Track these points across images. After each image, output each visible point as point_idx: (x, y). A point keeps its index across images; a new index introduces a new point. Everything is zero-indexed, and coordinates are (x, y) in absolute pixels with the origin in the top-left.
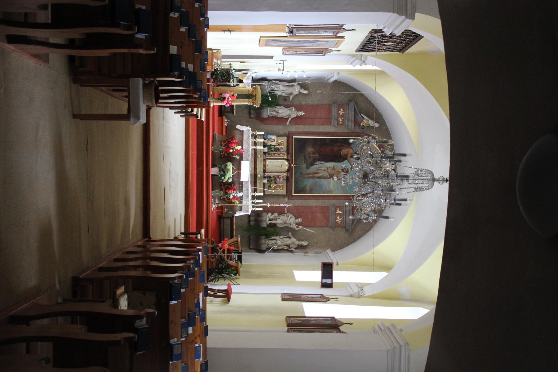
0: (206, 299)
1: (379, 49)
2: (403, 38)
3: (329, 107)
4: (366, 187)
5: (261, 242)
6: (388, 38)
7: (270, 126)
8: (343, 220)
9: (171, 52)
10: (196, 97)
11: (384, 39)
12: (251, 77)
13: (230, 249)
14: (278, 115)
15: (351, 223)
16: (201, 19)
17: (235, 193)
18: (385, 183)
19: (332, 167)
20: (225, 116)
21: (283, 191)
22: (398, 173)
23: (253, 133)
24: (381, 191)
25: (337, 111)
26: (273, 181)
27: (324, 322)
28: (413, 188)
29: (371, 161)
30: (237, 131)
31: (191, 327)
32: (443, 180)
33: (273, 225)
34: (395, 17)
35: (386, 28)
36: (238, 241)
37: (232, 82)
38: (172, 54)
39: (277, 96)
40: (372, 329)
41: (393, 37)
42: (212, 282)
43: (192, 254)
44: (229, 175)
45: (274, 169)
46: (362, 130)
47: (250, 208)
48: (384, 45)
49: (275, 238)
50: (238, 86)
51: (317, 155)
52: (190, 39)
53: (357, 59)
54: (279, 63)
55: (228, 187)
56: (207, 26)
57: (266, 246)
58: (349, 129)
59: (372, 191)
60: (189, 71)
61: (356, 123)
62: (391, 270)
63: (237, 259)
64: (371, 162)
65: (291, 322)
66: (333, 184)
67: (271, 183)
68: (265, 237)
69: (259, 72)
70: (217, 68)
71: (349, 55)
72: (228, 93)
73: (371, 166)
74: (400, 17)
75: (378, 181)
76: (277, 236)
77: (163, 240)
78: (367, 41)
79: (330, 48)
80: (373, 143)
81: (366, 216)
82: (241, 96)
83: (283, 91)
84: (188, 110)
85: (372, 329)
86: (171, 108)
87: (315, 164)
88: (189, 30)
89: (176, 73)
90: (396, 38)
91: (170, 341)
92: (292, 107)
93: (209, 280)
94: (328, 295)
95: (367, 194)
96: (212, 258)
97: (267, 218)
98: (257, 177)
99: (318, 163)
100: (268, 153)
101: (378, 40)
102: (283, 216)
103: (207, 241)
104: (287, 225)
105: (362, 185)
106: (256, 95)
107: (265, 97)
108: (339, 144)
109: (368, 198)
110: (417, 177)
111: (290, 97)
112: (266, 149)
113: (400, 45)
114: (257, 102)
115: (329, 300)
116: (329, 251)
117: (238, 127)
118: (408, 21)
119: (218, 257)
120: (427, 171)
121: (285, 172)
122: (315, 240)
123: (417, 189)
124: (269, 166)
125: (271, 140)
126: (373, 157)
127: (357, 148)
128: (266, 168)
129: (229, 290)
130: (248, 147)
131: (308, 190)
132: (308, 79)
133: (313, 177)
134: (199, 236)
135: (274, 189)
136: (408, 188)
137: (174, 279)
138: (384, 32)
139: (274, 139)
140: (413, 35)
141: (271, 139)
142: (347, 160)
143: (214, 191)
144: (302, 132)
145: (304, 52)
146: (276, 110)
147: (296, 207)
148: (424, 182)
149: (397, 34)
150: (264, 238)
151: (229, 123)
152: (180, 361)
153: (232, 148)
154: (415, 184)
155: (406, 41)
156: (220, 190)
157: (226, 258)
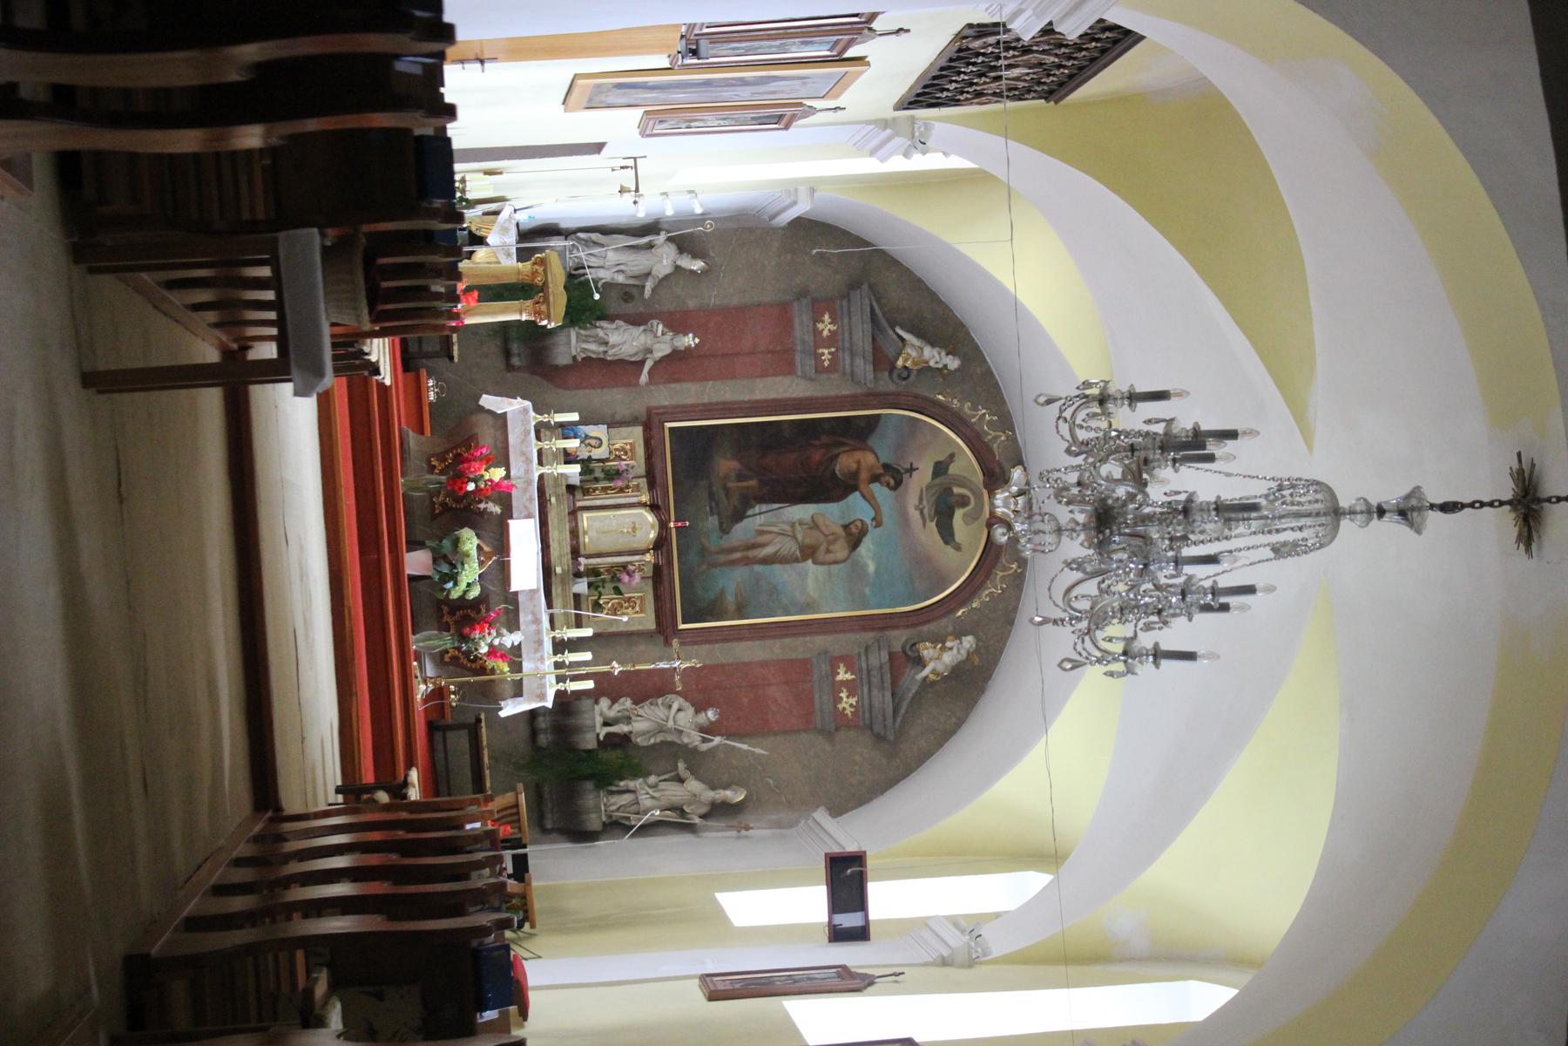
1: (979, 94)
3: (784, 309)
6: (1016, 53)
7: (580, 393)
8: (863, 706)
12: (514, 222)
14: (605, 352)
15: (891, 713)
17: (495, 634)
23: (540, 418)
25: (811, 325)
26: (609, 586)
32: (1369, 512)
33: (617, 740)
36: (517, 805)
41: (1035, 48)
43: (468, 849)
44: (470, 573)
45: (606, 544)
46: (904, 383)
47: (551, 685)
49: (631, 784)
50: (469, 258)
51: (753, 483)
53: (897, 134)
54: (622, 168)
55: (466, 616)
57: (600, 817)
61: (882, 361)
68: (595, 784)
69: (540, 204)
71: (868, 122)
76: (634, 779)
79: (808, 103)
87: (750, 512)
90: (1043, 52)
92: (655, 322)
97: (598, 719)
99: (757, 509)
100: (581, 487)
102: (652, 707)
104: (670, 738)
106: (545, 284)
108: (825, 439)
111: (644, 287)
114: (552, 310)
115: (871, 984)
116: (821, 815)
117: (488, 401)
121: (648, 551)
123: (1282, 549)
125: (587, 441)
128: (581, 539)
131: (732, 607)
132: (700, 220)
133: (748, 561)
139: (601, 437)
140: (1107, 34)
141: (587, 437)
142: (857, 494)
143: (418, 636)
144: (693, 406)
145: (716, 123)
146: (597, 335)
148: (1303, 521)
149: (1069, 33)
151: (442, 388)
153: (472, 476)
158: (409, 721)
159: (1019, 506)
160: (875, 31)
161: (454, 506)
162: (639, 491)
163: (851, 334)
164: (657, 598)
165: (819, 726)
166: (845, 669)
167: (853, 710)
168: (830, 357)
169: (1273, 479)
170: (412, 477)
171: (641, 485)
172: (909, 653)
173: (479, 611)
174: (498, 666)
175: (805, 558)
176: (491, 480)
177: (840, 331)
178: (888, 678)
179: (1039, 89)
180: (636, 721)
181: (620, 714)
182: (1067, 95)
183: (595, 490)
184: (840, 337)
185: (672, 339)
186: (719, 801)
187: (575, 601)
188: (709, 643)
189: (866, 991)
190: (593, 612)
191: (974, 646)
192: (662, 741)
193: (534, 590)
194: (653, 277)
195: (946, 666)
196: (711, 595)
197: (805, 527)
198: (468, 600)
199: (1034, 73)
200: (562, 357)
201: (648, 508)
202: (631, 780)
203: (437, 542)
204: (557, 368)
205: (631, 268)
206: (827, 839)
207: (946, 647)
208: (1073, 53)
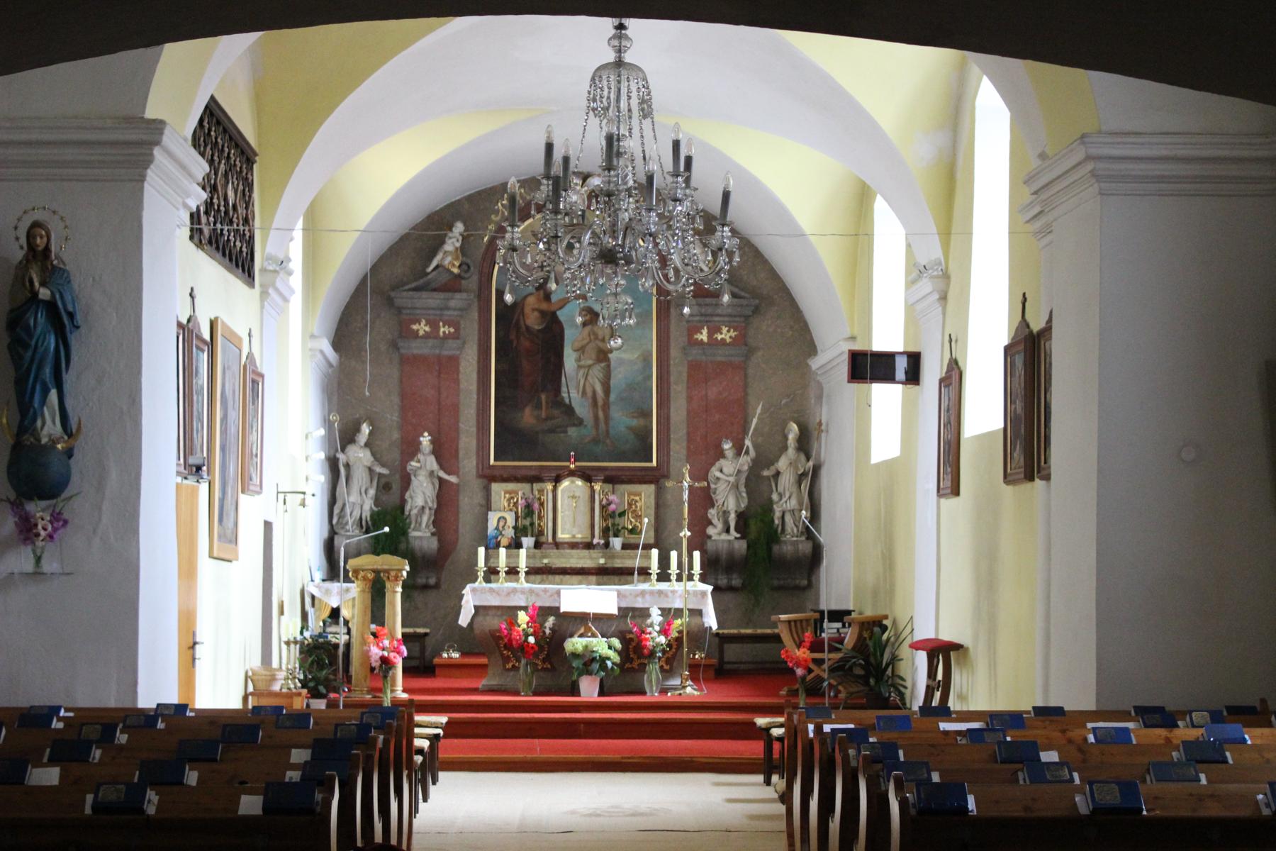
0: (957, 712)
2: (216, 154)
3: (406, 361)
4: (639, 256)
5: (788, 556)
6: (216, 197)
7: (461, 530)
8: (729, 322)
10: (384, 739)
11: (219, 206)
13: (811, 642)
14: (430, 509)
16: (161, 725)
18: (629, 203)
19: (579, 353)
20: (434, 657)
21: (645, 495)
22: (600, 164)
23: (480, 579)
24: (653, 214)
26: (617, 520)
27: (1020, 376)
28: (641, 123)
29: (565, 243)
31: (1039, 757)
36: (789, 622)
38: (264, 809)
40: (1039, 240)
41: (213, 182)
43: (830, 750)
44: (604, 647)
45: (584, 520)
46: (472, 268)
47: (695, 586)
48: (234, 207)
49: (777, 514)
51: (543, 397)
52: (218, 758)
53: (273, 285)
54: (285, 503)
55: (634, 651)
56: (181, 708)
57: (802, 542)
59: (651, 239)
60: (309, 759)
61: (452, 285)
62: (869, 187)
63: (839, 625)
64: (569, 242)
65: (1020, 470)
67: (624, 528)
69: (309, 560)
70: (299, 680)
71: (262, 307)
72: (370, 650)
73: (579, 242)
75: (624, 223)
77: (790, 835)
78: (224, 255)
80: (517, 235)
81: (722, 256)
82: (377, 612)
83: (364, 494)
84: (419, 762)
85: (1039, 240)
86: (414, 810)
87: (567, 401)
88: (194, 760)
89: (318, 797)
90: (216, 174)
91: (1084, 815)
92: (409, 468)
93: (902, 704)
95: (659, 253)
96: (836, 696)
97: (722, 537)
99: (565, 395)
102: (717, 492)
103: (791, 710)
104: (743, 481)
105: (633, 266)
109: (672, 251)
111: (380, 474)
112: (528, 541)
113: (235, 161)
115: (956, 362)
116: (815, 363)
117: (464, 620)
118: (168, 138)
119: (833, 678)
120: (595, 83)
121: (592, 488)
122: (784, 402)
123: (646, 112)
124: (574, 533)
125: (501, 528)
126: (556, 237)
127: (529, 281)
128: (579, 540)
129: (929, 646)
132: (328, 424)
133: (606, 405)
134: (777, 732)
135: (639, 517)
136: (642, 136)
137: (903, 804)
138: (198, 208)
141: (497, 528)
142: (558, 313)
143: (648, 690)
144: (478, 440)
147: (691, 456)
148: (624, 91)
149: (204, 170)
150: (778, 547)
152: (1140, 786)
153: (523, 638)
154: (630, 117)
155: (223, 146)
159: (578, 182)
160: (190, 316)
162: (543, 491)
163: (429, 309)
164: (630, 481)
165: (743, 359)
166: (699, 334)
168: (447, 327)
169: (587, 113)
170: (520, 686)
171: (539, 488)
173: (631, 639)
175: (607, 360)
176: (528, 623)
178: (708, 300)
179: (245, 171)
180: (727, 507)
182: (248, 143)
183: (539, 525)
184: (432, 317)
185: (423, 454)
187: (627, 549)
188: (670, 442)
189: (962, 368)
192: (745, 487)
193: (618, 594)
194: (373, 465)
196: (632, 437)
197: (582, 357)
198: (622, 648)
199: (232, 178)
201: (558, 484)
202: (774, 514)
203: (574, 670)
204: (439, 549)
205: (364, 483)
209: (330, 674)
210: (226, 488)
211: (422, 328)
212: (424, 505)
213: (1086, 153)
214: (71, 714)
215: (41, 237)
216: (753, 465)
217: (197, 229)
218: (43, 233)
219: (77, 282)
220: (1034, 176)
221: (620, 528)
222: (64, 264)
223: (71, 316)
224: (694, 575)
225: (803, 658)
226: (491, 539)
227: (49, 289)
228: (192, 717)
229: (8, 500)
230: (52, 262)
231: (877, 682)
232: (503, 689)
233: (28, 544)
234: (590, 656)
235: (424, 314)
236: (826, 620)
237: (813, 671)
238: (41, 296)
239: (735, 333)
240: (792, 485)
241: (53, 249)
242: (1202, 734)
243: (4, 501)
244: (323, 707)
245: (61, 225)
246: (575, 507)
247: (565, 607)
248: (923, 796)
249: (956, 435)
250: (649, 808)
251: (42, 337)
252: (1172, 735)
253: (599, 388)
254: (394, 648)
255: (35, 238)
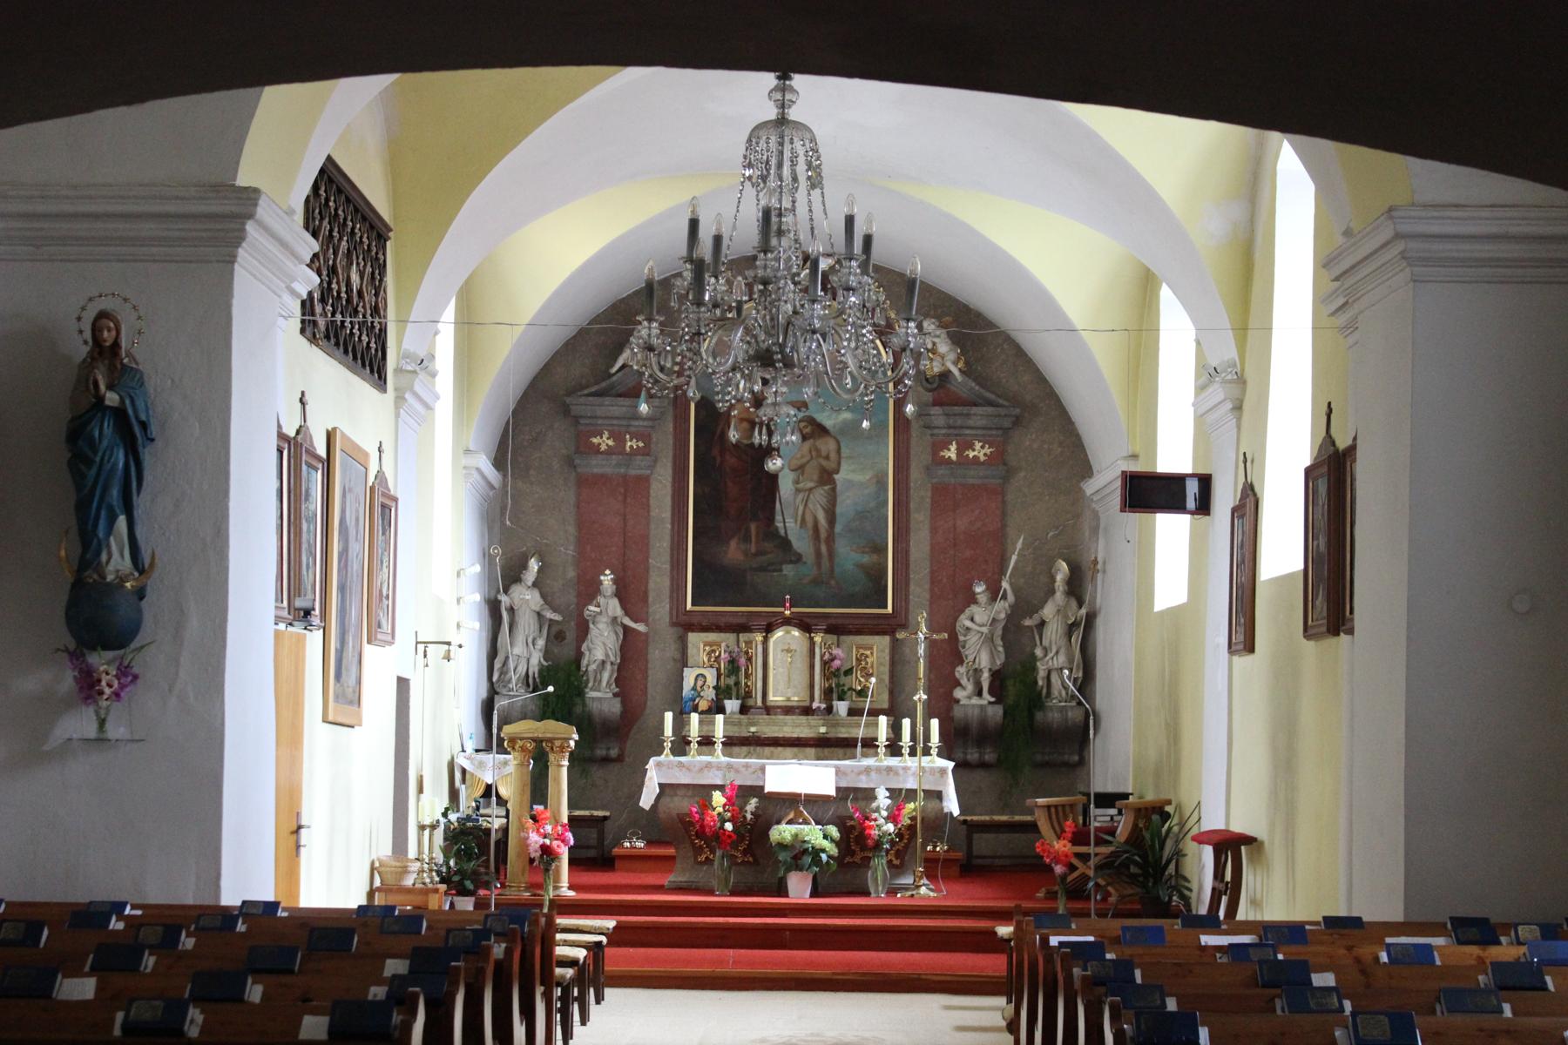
1: (376, 311)
3: (583, 482)
5: (1055, 726)
6: (335, 281)
7: (650, 690)
8: (983, 435)
9: (322, 1035)
10: (506, 948)
11: (339, 292)
13: (1073, 833)
14: (612, 663)
16: (241, 927)
17: (876, 814)
21: (878, 647)
23: (667, 751)
26: (843, 679)
27: (1323, 505)
28: (809, 194)
30: (659, 805)
31: (1310, 980)
34: (250, 254)
35: (293, 285)
36: (1048, 807)
37: (488, 822)
38: (330, 1033)
39: (545, 664)
40: (1346, 337)
41: (331, 262)
42: (1190, 898)
44: (814, 835)
45: (801, 678)
49: (1042, 674)
51: (753, 527)
52: (297, 968)
54: (425, 656)
55: (855, 841)
56: (272, 907)
57: (1072, 707)
58: (663, 413)
62: (1154, 274)
63: (1113, 811)
66: (853, 471)
67: (851, 689)
68: (1039, 711)
71: (397, 415)
72: (528, 838)
74: (247, 240)
82: (538, 789)
85: (1346, 337)
87: (782, 532)
88: (258, 972)
89: (396, 1018)
90: (335, 254)
94: (1235, 491)
96: (1104, 899)
97: (971, 700)
98: (828, 736)
99: (780, 525)
101: (342, 313)
102: (967, 647)
104: (999, 632)
106: (534, 740)
107: (548, 708)
108: (715, 452)
109: (843, 351)
110: (773, 183)
111: (551, 620)
112: (732, 705)
115: (1252, 487)
116: (1090, 487)
117: (647, 800)
118: (263, 211)
119: (1102, 878)
121: (811, 639)
122: (1051, 534)
124: (789, 695)
125: (699, 689)
126: (699, 334)
128: (795, 704)
129: (1216, 838)
130: (719, 768)
131: (875, 557)
132: (487, 559)
133: (831, 539)
138: (310, 294)
139: (695, 676)
140: (322, 192)
141: (694, 688)
143: (872, 890)
144: (672, 579)
146: (595, 671)
148: (787, 154)
149: (312, 250)
151: (634, 834)
153: (719, 825)
155: (345, 219)
156: (868, 867)
157: (1105, 850)
158: (948, 911)
160: (301, 426)
161: (747, 842)
162: (751, 642)
164: (859, 632)
165: (1000, 481)
167: (987, 446)
168: (635, 440)
170: (714, 883)
171: (746, 639)
172: (935, 385)
173: (853, 827)
174: (909, 813)
175: (833, 482)
176: (724, 806)
177: (610, 428)
178: (957, 409)
179: (374, 250)
180: (979, 664)
181: (971, 679)
185: (604, 596)
186: (1066, 588)
189: (1259, 495)
190: (867, 697)
191: (933, 320)
194: (542, 610)
195: (951, 350)
198: (841, 837)
199: (358, 258)
200: (614, 708)
201: (769, 635)
202: (1037, 673)
203: (781, 865)
204: (624, 713)
206: (1107, 491)
207: (933, 349)
208: (339, 222)
209: (478, 866)
210: (346, 637)
211: (604, 441)
212: (604, 658)
213: (1395, 229)
214: (139, 912)
215: (109, 331)
216: (1012, 611)
217: (309, 320)
218: (112, 325)
219: (152, 383)
220: (1335, 258)
221: (846, 689)
222: (137, 363)
223: (144, 426)
224: (931, 748)
225: (1063, 851)
226: (686, 702)
227: (116, 392)
228: (285, 917)
229: (67, 650)
230: (122, 359)
231: (1155, 883)
232: (693, 887)
233: (90, 704)
234: (801, 847)
235: (608, 425)
236: (1092, 806)
237: (1076, 868)
238: (107, 402)
239: (991, 450)
240: (1060, 638)
241: (123, 345)
242: (1524, 954)
243: (63, 651)
244: (471, 908)
245: (134, 315)
246: (790, 663)
247: (769, 788)
248: (1143, 1027)
249: (1251, 582)
250: (857, 1036)
251: (108, 453)
252: (1486, 955)
253: (821, 516)
254: (558, 835)
255: (101, 331)
